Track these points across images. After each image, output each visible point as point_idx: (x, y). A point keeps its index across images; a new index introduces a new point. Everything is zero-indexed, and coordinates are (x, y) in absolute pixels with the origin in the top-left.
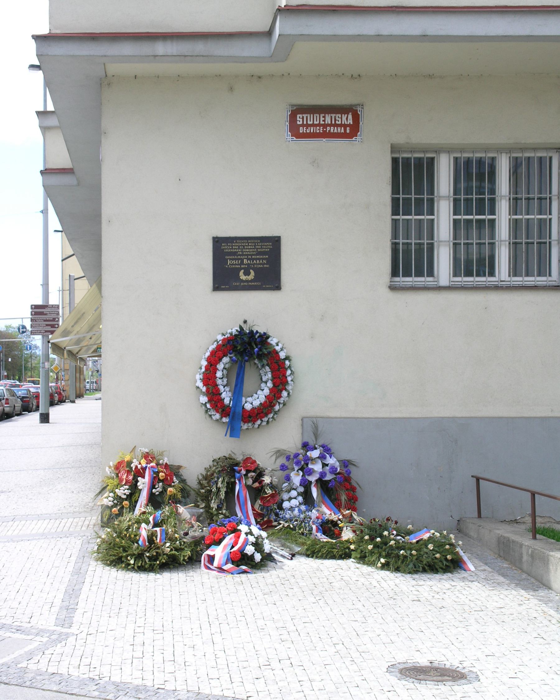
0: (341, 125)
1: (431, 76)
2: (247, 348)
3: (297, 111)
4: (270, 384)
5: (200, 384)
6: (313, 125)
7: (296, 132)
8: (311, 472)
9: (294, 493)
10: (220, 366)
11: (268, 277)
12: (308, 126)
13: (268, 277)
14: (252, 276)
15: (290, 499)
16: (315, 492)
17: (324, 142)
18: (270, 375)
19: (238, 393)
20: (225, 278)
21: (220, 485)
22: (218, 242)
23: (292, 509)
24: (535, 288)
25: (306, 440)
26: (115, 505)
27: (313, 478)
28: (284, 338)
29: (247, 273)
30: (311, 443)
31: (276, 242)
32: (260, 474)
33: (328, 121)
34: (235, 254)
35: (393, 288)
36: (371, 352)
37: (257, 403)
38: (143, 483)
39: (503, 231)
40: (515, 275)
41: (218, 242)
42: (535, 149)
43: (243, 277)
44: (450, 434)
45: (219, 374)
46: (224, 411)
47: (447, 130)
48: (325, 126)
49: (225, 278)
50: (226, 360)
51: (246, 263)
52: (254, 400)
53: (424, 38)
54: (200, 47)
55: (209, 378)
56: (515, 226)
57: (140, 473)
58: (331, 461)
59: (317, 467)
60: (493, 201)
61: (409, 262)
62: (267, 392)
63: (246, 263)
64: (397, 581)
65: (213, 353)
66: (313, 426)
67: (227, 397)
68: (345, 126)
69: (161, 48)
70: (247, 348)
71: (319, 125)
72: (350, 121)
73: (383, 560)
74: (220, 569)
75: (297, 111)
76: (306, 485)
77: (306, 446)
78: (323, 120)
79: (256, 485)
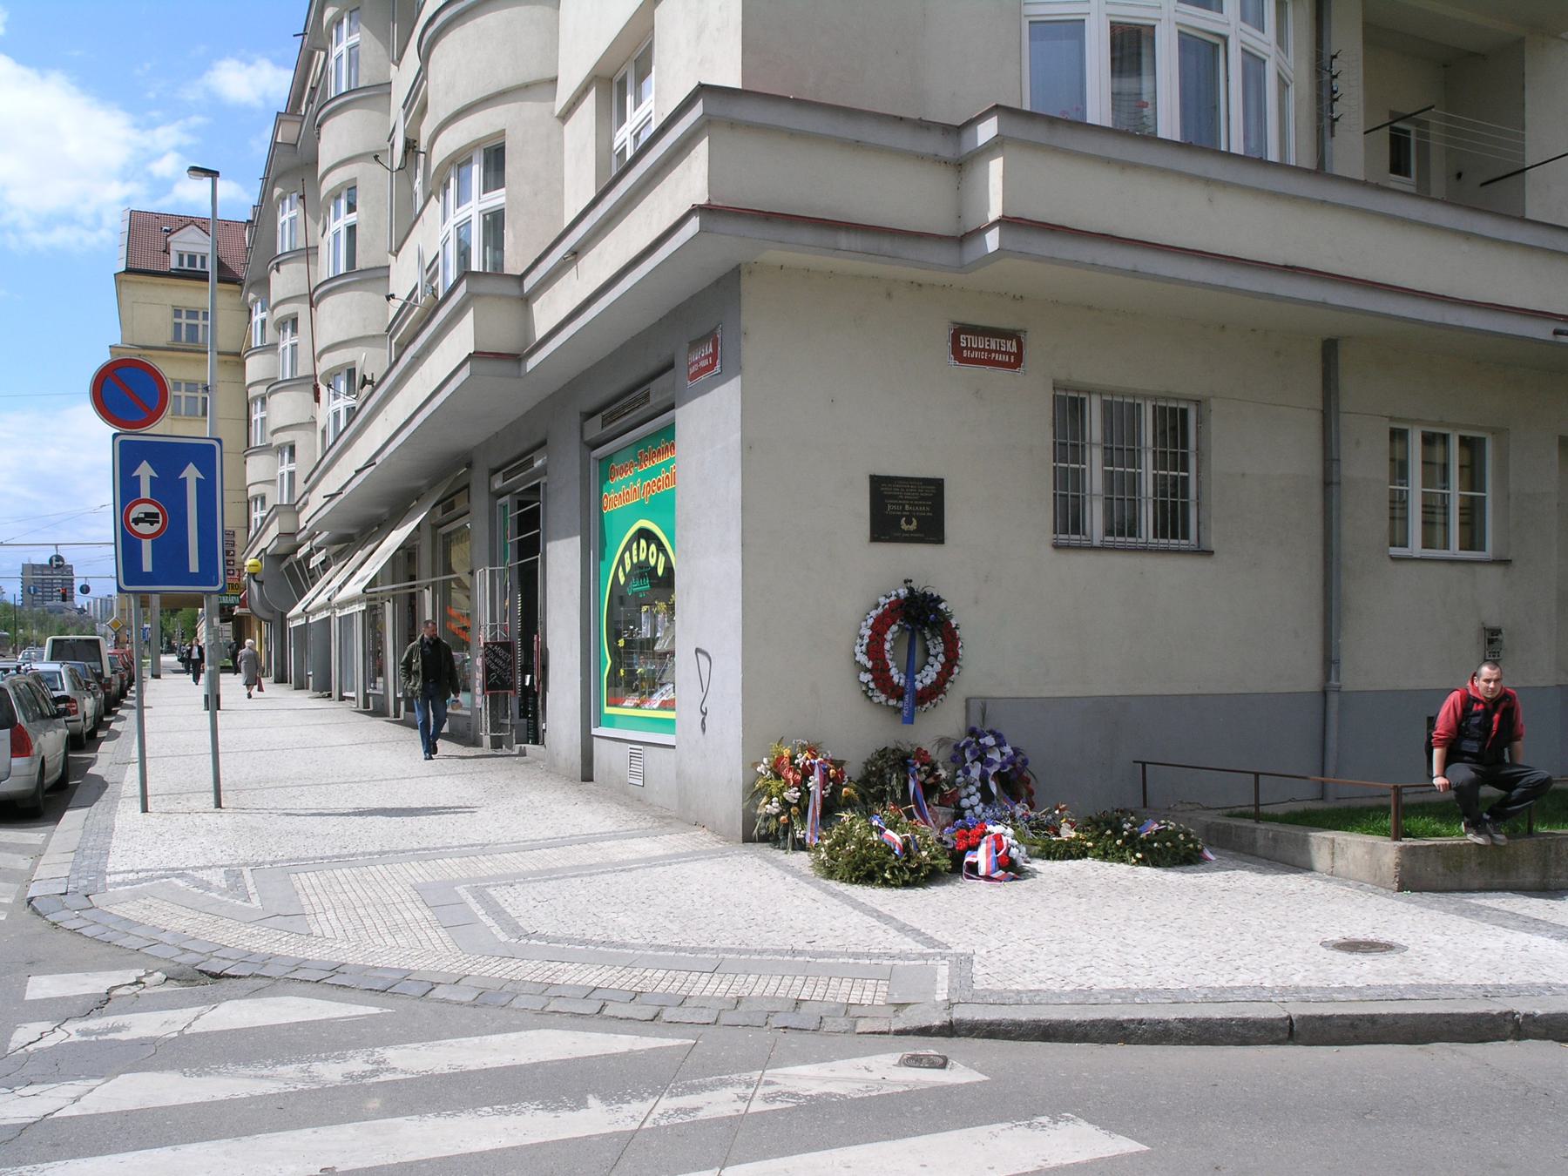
0: (1005, 353)
1: (1090, 308)
2: (918, 615)
3: (959, 330)
4: (941, 658)
5: (863, 659)
6: (978, 349)
7: (957, 352)
8: (991, 763)
9: (972, 789)
10: (889, 636)
11: (931, 530)
12: (972, 349)
13: (931, 530)
14: (913, 526)
15: (968, 796)
16: (994, 788)
17: (987, 370)
18: (941, 648)
19: (910, 671)
20: (884, 528)
21: (894, 782)
22: (877, 482)
23: (972, 807)
24: (1178, 551)
25: (972, 725)
26: (781, 813)
27: (992, 771)
28: (957, 607)
29: (909, 522)
30: (979, 729)
31: (937, 485)
32: (934, 769)
33: (993, 346)
34: (895, 497)
35: (1056, 546)
36: (1042, 619)
37: (928, 681)
38: (814, 782)
39: (1147, 487)
40: (1164, 536)
41: (877, 482)
42: (1177, 400)
43: (904, 527)
44: (1111, 713)
45: (887, 646)
46: (896, 692)
47: (1108, 369)
48: (990, 351)
49: (884, 528)
50: (894, 628)
51: (906, 510)
52: (928, 676)
53: (1134, 273)
54: (886, 245)
55: (875, 649)
56: (1109, 477)
57: (807, 772)
58: (1008, 749)
59: (995, 756)
60: (1185, 457)
61: (1069, 519)
62: (938, 667)
63: (906, 510)
64: (1201, 881)
65: (878, 620)
66: (979, 708)
67: (897, 677)
68: (1010, 354)
69: (844, 240)
70: (918, 615)
71: (984, 350)
72: (1015, 349)
73: (1139, 855)
74: (988, 878)
75: (959, 330)
76: (984, 778)
77: (972, 732)
78: (985, 344)
79: (931, 780)
